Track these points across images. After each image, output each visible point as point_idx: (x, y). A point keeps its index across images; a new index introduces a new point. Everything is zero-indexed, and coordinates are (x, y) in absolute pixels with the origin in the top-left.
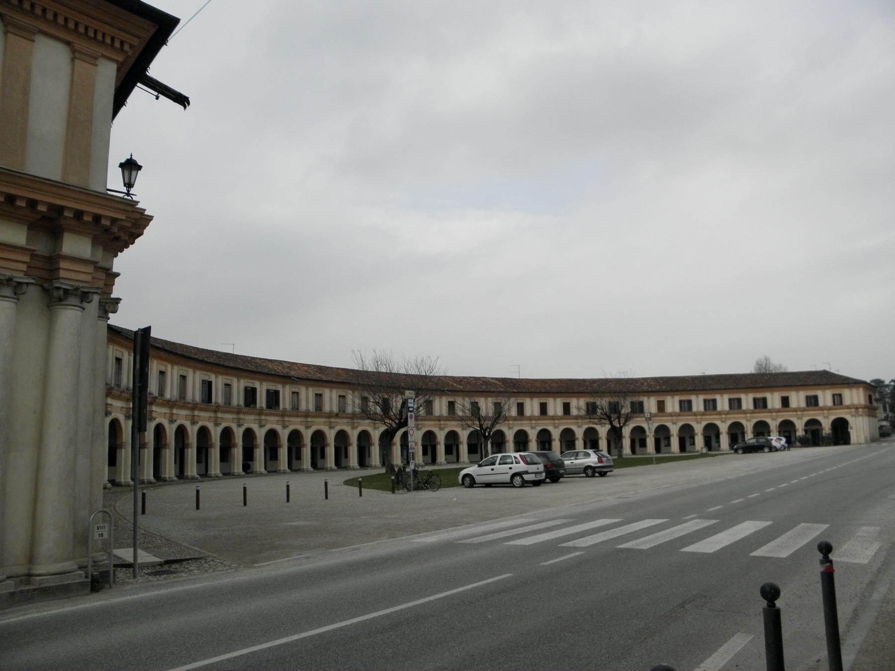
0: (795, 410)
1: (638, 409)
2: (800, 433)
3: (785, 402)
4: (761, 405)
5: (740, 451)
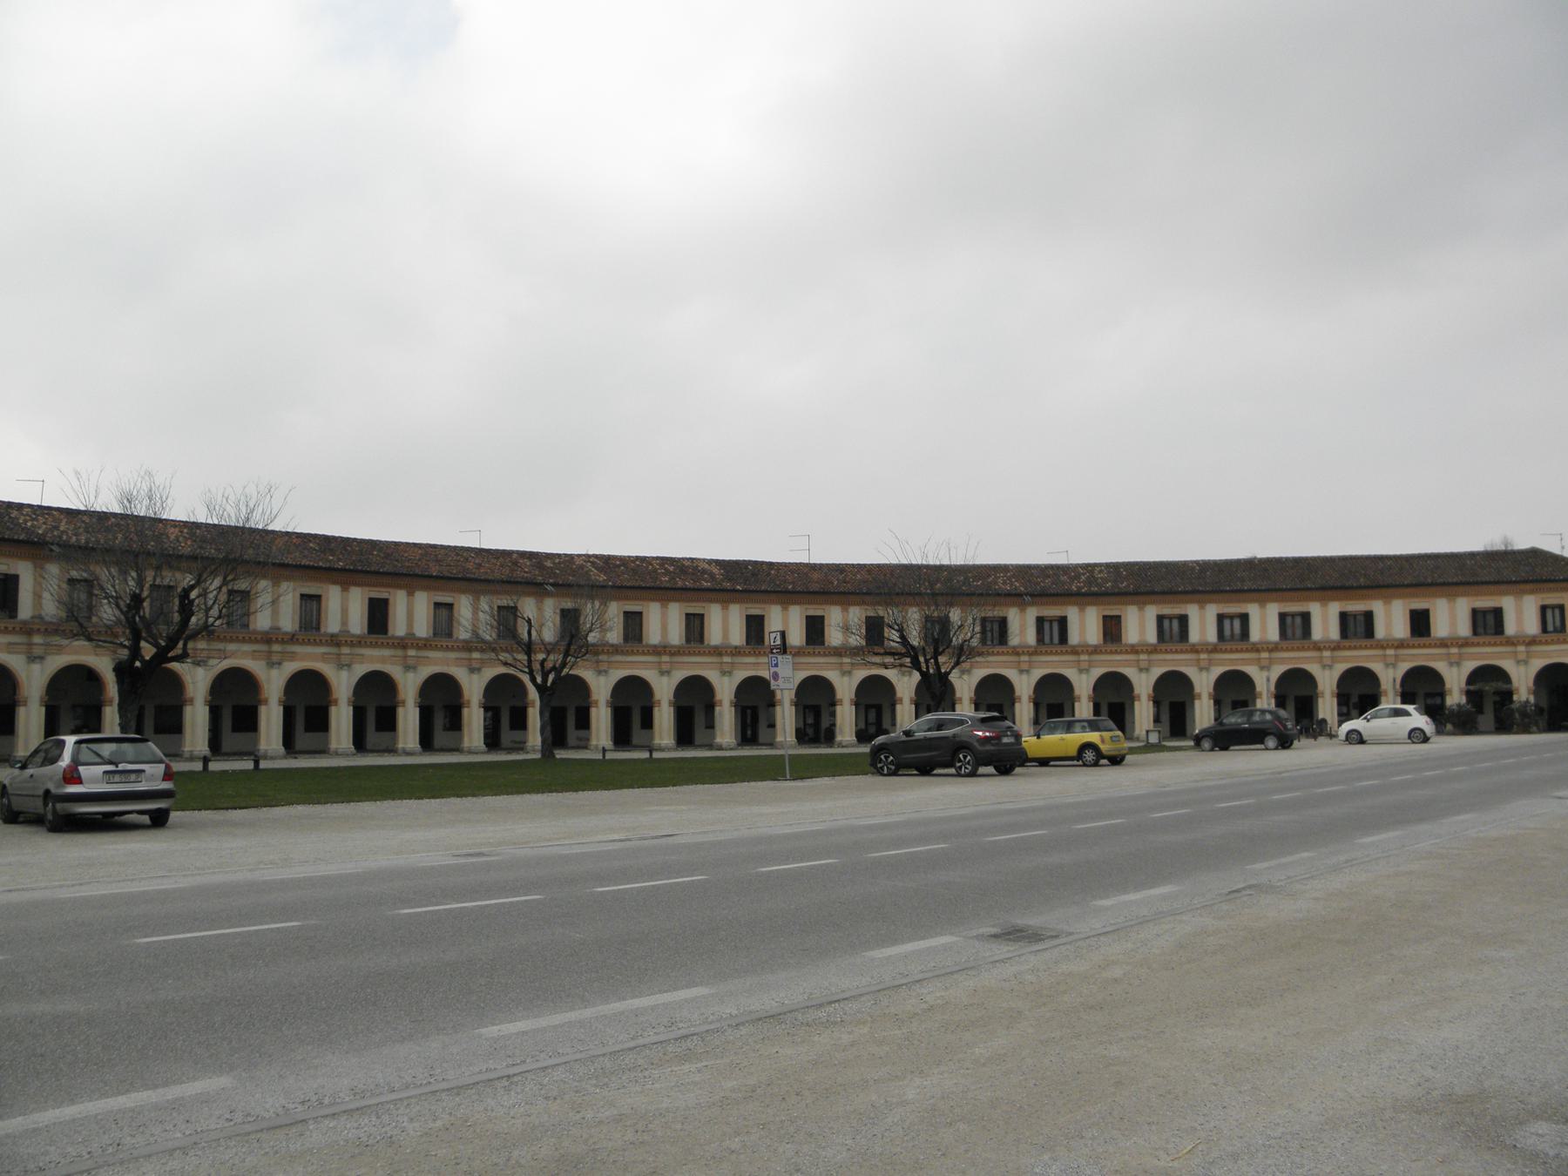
0: (1443, 643)
1: (997, 632)
2: (1455, 697)
3: (1420, 623)
4: (1361, 629)
5: (1206, 744)
